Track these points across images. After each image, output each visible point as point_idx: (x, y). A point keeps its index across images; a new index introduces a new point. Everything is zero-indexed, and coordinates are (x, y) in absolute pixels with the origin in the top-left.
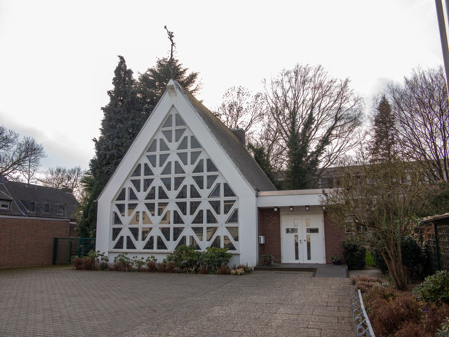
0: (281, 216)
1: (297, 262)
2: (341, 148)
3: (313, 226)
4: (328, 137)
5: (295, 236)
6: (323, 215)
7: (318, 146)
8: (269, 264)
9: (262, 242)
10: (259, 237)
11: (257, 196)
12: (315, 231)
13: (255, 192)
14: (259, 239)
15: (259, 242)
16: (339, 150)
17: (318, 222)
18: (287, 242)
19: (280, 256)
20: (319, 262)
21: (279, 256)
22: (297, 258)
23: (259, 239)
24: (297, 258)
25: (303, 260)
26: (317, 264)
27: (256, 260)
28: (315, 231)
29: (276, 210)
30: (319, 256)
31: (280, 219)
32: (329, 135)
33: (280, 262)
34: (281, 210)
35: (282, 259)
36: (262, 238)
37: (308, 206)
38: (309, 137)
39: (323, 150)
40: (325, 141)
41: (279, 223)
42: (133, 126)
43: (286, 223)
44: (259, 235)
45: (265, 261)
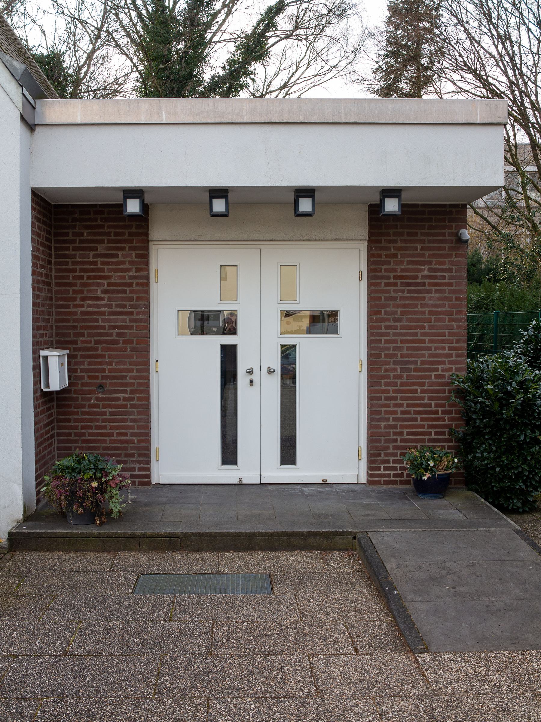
0: (153, 247)
1: (229, 475)
2: (292, 80)
3: (310, 301)
4: (262, 34)
5: (224, 348)
6: (364, 246)
7: (231, 62)
8: (97, 512)
9: (56, 382)
10: (36, 358)
11: (30, 125)
12: (323, 322)
13: (15, 91)
14: (39, 368)
15: (37, 382)
16: (285, 86)
17: (338, 277)
18: (180, 377)
19: (148, 449)
20: (335, 476)
21: (139, 449)
22: (229, 456)
23: (36, 368)
24: (229, 456)
25: (259, 463)
26: (325, 484)
27: (18, 491)
28: (323, 322)
29: (133, 206)
30: (336, 448)
31: (147, 264)
32: (267, 28)
33: (144, 479)
34: (155, 215)
35: (154, 466)
36: (56, 361)
37: (307, 192)
38: (208, 26)
39: (246, 74)
40: (254, 47)
41: (147, 285)
42: (76, 371)
43: (180, 279)
44: (39, 344)
45: (72, 497)
